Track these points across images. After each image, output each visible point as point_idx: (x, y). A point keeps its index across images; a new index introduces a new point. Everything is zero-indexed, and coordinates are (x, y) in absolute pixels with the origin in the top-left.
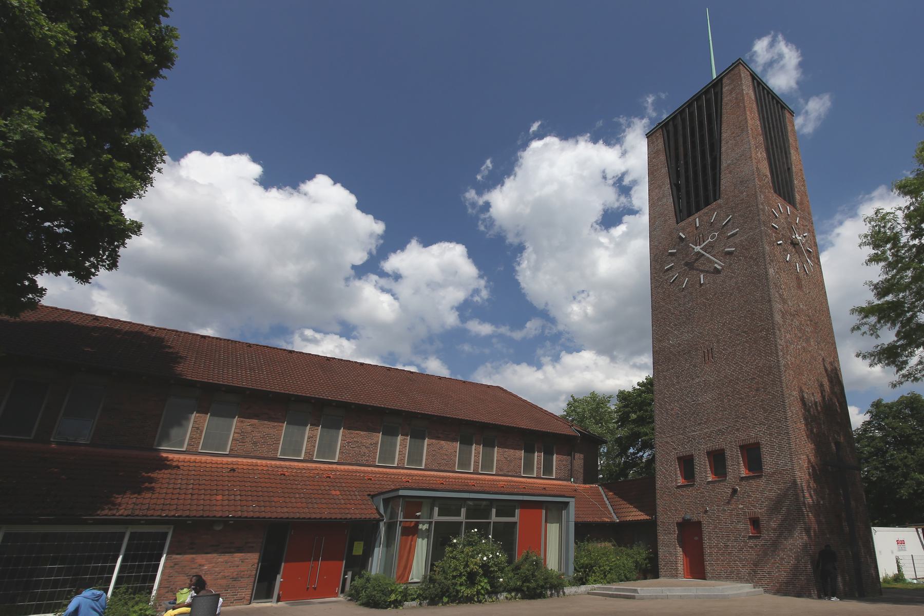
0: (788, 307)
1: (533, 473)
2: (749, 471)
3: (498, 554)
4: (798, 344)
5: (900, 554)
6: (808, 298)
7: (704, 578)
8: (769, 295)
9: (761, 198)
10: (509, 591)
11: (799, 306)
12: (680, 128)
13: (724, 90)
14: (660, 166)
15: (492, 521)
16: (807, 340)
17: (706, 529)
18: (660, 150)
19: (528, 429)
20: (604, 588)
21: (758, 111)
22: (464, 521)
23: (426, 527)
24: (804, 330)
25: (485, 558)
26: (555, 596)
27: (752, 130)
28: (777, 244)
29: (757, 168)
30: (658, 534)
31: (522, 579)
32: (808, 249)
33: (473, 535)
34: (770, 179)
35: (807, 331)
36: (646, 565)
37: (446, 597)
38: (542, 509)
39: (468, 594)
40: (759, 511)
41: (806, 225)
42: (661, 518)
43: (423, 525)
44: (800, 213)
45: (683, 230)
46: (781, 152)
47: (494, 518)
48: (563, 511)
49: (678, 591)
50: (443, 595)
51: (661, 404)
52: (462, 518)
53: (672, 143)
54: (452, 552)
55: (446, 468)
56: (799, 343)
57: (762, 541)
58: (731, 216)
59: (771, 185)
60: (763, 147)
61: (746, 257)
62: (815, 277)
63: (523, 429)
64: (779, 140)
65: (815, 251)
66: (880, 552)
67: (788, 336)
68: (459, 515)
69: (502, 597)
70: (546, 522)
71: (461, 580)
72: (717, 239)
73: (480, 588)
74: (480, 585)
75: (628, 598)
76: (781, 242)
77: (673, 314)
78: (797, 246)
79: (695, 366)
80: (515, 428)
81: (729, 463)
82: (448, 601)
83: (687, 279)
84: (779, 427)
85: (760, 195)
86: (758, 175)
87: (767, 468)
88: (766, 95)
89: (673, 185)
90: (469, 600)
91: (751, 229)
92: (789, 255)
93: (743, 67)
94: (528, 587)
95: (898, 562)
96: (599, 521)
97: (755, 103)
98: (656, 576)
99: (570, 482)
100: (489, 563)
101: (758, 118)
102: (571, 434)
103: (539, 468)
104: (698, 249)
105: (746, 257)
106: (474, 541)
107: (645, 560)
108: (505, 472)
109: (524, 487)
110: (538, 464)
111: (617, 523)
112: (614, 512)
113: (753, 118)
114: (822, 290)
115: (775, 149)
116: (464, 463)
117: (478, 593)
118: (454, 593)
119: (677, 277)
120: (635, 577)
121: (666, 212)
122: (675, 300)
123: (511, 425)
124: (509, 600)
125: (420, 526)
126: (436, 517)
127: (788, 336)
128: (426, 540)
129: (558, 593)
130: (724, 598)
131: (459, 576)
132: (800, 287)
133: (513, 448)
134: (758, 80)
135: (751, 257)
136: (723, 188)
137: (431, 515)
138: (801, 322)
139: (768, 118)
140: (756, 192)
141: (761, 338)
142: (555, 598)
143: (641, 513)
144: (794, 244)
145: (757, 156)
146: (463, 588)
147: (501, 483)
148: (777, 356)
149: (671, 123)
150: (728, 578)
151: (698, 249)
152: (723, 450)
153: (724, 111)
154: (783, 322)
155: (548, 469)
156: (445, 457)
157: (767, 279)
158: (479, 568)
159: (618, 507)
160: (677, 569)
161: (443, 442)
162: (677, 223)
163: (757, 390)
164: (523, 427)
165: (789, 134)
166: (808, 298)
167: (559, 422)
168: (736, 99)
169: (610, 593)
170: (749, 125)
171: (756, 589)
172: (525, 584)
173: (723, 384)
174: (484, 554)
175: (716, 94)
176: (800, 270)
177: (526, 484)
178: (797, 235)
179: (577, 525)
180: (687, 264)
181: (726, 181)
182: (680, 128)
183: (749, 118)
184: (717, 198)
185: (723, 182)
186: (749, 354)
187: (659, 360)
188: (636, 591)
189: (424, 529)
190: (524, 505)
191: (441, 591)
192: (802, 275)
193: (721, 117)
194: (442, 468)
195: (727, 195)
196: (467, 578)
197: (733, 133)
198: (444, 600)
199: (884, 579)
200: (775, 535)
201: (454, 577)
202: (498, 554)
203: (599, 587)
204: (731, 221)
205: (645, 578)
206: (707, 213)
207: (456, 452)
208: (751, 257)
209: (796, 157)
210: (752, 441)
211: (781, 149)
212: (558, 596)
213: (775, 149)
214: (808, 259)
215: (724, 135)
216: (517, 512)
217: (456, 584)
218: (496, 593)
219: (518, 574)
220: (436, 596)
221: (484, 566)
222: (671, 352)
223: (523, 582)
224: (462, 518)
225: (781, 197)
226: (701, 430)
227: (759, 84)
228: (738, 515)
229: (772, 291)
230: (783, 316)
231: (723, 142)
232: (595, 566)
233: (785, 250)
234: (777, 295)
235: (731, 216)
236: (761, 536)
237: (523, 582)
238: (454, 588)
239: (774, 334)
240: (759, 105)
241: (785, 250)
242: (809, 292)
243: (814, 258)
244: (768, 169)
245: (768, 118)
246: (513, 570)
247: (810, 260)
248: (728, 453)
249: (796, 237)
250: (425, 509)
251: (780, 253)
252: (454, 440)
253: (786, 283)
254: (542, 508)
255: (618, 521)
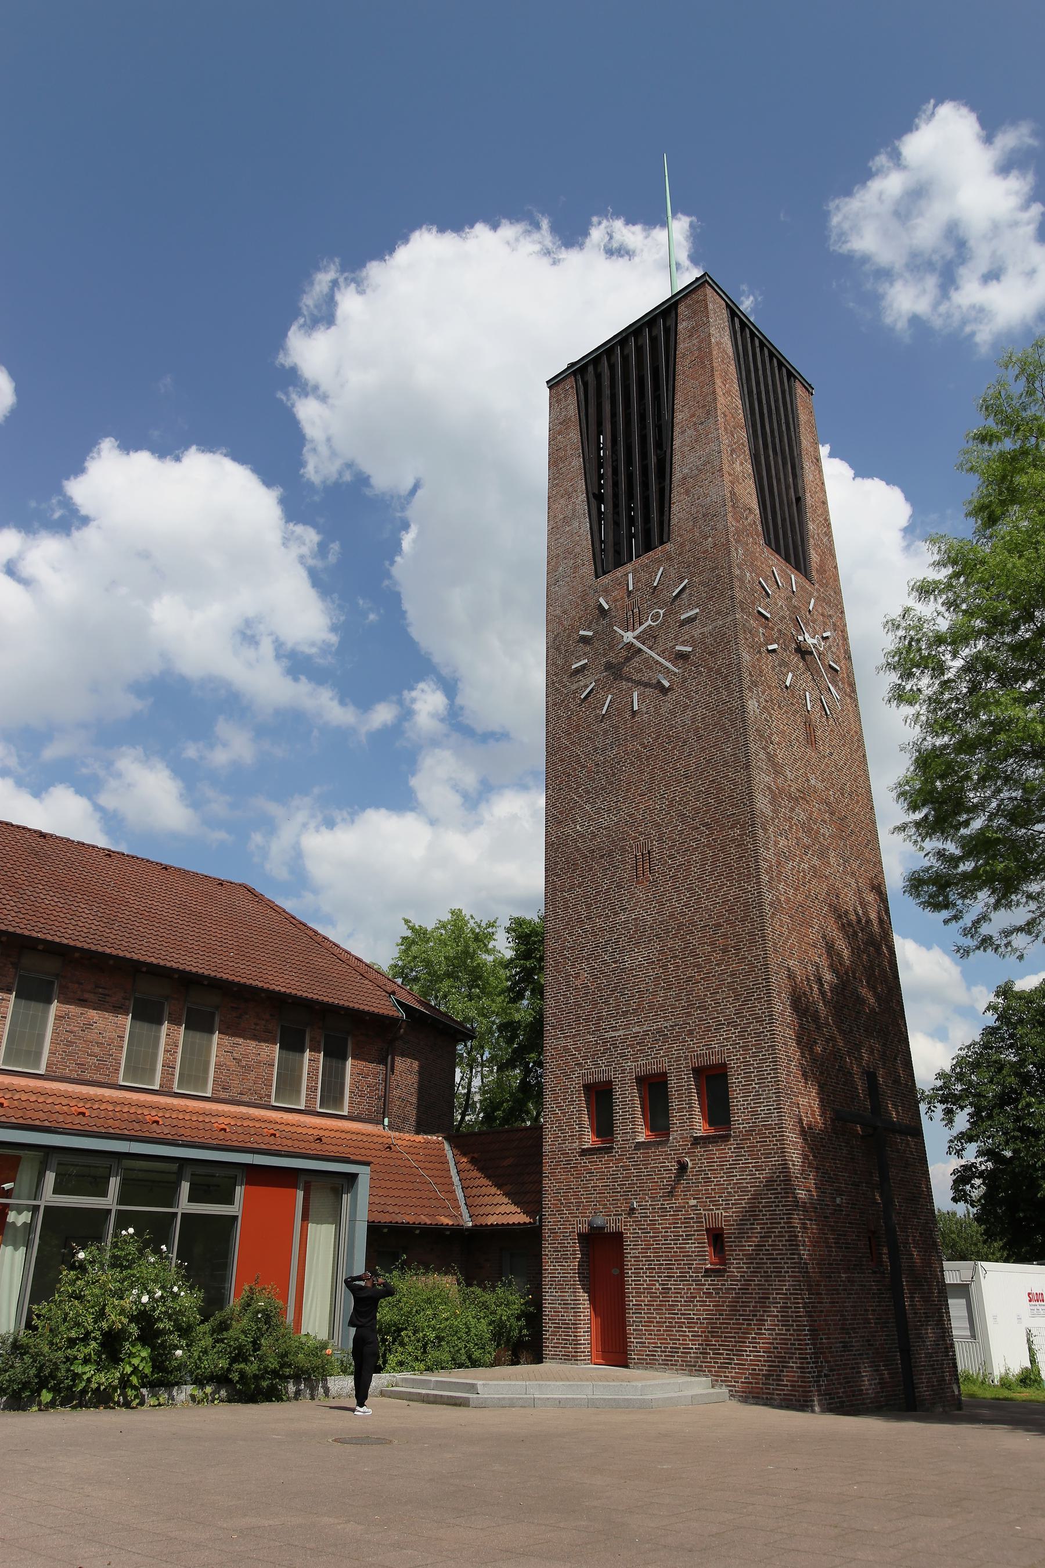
0: (786, 780)
1: (298, 1100)
2: (710, 1126)
3: (175, 1289)
4: (802, 860)
5: (1034, 1324)
6: (827, 765)
7: (626, 1366)
8: (747, 755)
9: (738, 554)
10: (199, 1382)
11: (808, 780)
12: (606, 382)
13: (680, 327)
14: (570, 452)
15: (180, 1211)
16: (822, 854)
17: (632, 1252)
18: (570, 419)
19: (290, 995)
20: (413, 1380)
21: (740, 379)
22: (115, 1207)
23: (25, 1217)
24: (817, 832)
25: (145, 1299)
26: (305, 1397)
27: (725, 416)
28: (767, 650)
29: (733, 493)
30: (545, 1259)
31: (230, 1353)
32: (831, 663)
33: (125, 1241)
34: (758, 516)
35: (824, 835)
36: (520, 1332)
37: (49, 1390)
38: (296, 1187)
39: (100, 1384)
40: (726, 1215)
41: (830, 616)
42: (550, 1222)
43: (20, 1213)
44: (818, 591)
45: (606, 592)
46: (784, 464)
47: (185, 1205)
48: (345, 1196)
49: (586, 1391)
50: (43, 1384)
51: (557, 963)
52: (110, 1201)
53: (592, 410)
54: (73, 1283)
55: (97, 1077)
56: (806, 858)
57: (727, 1281)
58: (686, 581)
59: (760, 528)
60: (747, 452)
61: (710, 670)
62: (844, 722)
63: (279, 993)
64: (781, 441)
65: (847, 669)
66: (995, 1318)
67: (782, 842)
68: (104, 1194)
69: (182, 1397)
70: (305, 1217)
71: (87, 1351)
72: (662, 624)
73: (129, 1369)
74: (130, 1363)
75: (455, 1405)
76: (775, 646)
77: (583, 767)
78: (808, 657)
79: (619, 886)
80: (262, 989)
81: (674, 1104)
82: (54, 1399)
83: (610, 697)
84: (758, 1035)
85: (736, 549)
86: (733, 506)
87: (740, 1120)
88: (758, 350)
89: (591, 495)
90: (102, 1399)
91: (719, 612)
92: (790, 675)
93: (711, 290)
94: (242, 1374)
95: (1029, 1342)
96: (429, 1222)
97: (733, 362)
98: (538, 1359)
99: (381, 1127)
100: (154, 1310)
101: (738, 394)
102: (386, 1012)
103: (311, 1089)
104: (629, 637)
105: (710, 670)
106: (125, 1258)
107: (518, 1319)
108: (233, 1093)
109: (272, 1131)
110: (309, 1078)
111: (468, 1229)
112: (466, 1204)
113: (728, 392)
114: (856, 751)
115: (771, 458)
116: (140, 1065)
117: (125, 1382)
118: (69, 1382)
119: (592, 689)
120: (488, 1358)
121: (578, 549)
122: (589, 738)
123: (251, 981)
124: (199, 1403)
125: (12, 1217)
126: (49, 1197)
127: (782, 842)
128: (22, 1250)
129: (313, 1389)
130: (644, 1406)
131: (82, 1340)
132: (811, 739)
133: (255, 1038)
134: (742, 317)
135: (719, 672)
136: (674, 521)
137: (37, 1191)
138: (811, 814)
139: (759, 393)
140: (728, 541)
141: (733, 841)
142: (305, 1402)
143: (513, 1208)
144: (803, 652)
145: (733, 469)
146: (89, 1370)
147: (221, 1120)
148: (758, 883)
149: (591, 369)
150: (668, 1364)
151: (629, 637)
152: (664, 1075)
153: (679, 368)
154: (773, 811)
155: (332, 1092)
156: (97, 1050)
157: (744, 721)
158: (130, 1321)
159: (475, 1191)
160: (576, 1343)
161: (93, 1014)
162: (597, 577)
163: (725, 951)
164: (277, 989)
165: (802, 430)
166: (827, 765)
167: (366, 982)
168: (699, 349)
169: (424, 1392)
170: (719, 406)
171: (716, 1390)
172: (236, 1366)
173: (667, 932)
174: (145, 1289)
175: (667, 330)
176: (813, 706)
177: (278, 1127)
178: (807, 636)
179: (374, 1230)
180: (609, 666)
181: (680, 508)
182: (606, 382)
183: (719, 391)
184: (665, 540)
185: (675, 508)
186: (711, 873)
187: (556, 863)
188: (472, 1388)
189: (19, 1224)
190: (257, 1175)
191: (37, 1376)
192: (816, 716)
193: (674, 380)
194: (87, 1076)
195: (681, 536)
196: (102, 1345)
197: (693, 416)
198: (42, 1398)
199: (1001, 1379)
200: (750, 1268)
201: (72, 1342)
202: (175, 1289)
203: (405, 1380)
204: (687, 591)
205: (515, 1362)
206: (646, 565)
207: (122, 1037)
208: (719, 672)
209: (814, 476)
210: (714, 1060)
211: (784, 459)
212: (313, 1398)
213: (771, 458)
214: (830, 685)
215: (679, 417)
216: (239, 1191)
217: (76, 1358)
218: (169, 1385)
219: (222, 1341)
220: (25, 1385)
221: (144, 1318)
222: (578, 850)
223: (234, 1360)
224: (110, 1201)
225: (780, 555)
226: (627, 1027)
227: (743, 325)
228: (687, 1221)
229: (753, 747)
230: (774, 801)
231: (677, 430)
232: (406, 1329)
233: (783, 663)
234: (762, 755)
235: (686, 581)
236: (725, 1271)
237: (234, 1360)
238: (68, 1370)
239: (754, 835)
240: (743, 366)
241: (783, 663)
242: (831, 754)
243: (843, 683)
244: (755, 496)
245: (759, 393)
246: (213, 1331)
247: (836, 686)
248: (673, 1082)
249: (805, 640)
250: (26, 1175)
251: (773, 668)
252: (118, 1009)
253: (783, 732)
254: (295, 1186)
255: (470, 1224)
